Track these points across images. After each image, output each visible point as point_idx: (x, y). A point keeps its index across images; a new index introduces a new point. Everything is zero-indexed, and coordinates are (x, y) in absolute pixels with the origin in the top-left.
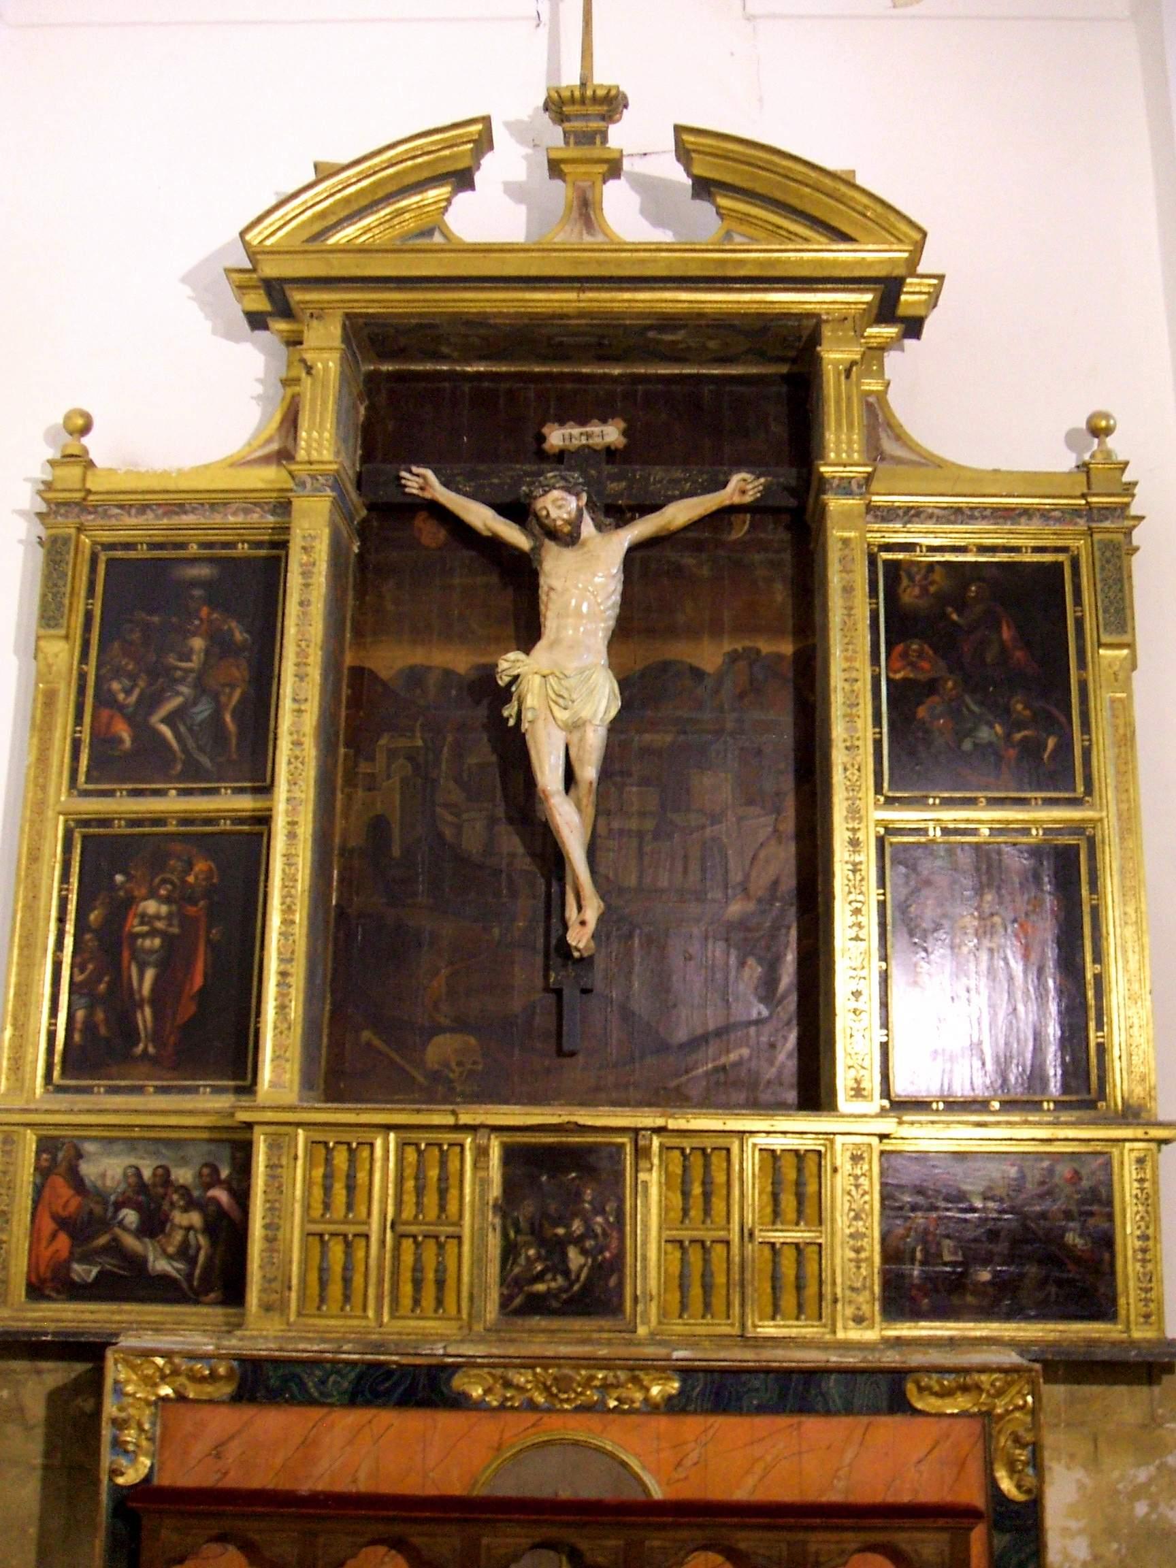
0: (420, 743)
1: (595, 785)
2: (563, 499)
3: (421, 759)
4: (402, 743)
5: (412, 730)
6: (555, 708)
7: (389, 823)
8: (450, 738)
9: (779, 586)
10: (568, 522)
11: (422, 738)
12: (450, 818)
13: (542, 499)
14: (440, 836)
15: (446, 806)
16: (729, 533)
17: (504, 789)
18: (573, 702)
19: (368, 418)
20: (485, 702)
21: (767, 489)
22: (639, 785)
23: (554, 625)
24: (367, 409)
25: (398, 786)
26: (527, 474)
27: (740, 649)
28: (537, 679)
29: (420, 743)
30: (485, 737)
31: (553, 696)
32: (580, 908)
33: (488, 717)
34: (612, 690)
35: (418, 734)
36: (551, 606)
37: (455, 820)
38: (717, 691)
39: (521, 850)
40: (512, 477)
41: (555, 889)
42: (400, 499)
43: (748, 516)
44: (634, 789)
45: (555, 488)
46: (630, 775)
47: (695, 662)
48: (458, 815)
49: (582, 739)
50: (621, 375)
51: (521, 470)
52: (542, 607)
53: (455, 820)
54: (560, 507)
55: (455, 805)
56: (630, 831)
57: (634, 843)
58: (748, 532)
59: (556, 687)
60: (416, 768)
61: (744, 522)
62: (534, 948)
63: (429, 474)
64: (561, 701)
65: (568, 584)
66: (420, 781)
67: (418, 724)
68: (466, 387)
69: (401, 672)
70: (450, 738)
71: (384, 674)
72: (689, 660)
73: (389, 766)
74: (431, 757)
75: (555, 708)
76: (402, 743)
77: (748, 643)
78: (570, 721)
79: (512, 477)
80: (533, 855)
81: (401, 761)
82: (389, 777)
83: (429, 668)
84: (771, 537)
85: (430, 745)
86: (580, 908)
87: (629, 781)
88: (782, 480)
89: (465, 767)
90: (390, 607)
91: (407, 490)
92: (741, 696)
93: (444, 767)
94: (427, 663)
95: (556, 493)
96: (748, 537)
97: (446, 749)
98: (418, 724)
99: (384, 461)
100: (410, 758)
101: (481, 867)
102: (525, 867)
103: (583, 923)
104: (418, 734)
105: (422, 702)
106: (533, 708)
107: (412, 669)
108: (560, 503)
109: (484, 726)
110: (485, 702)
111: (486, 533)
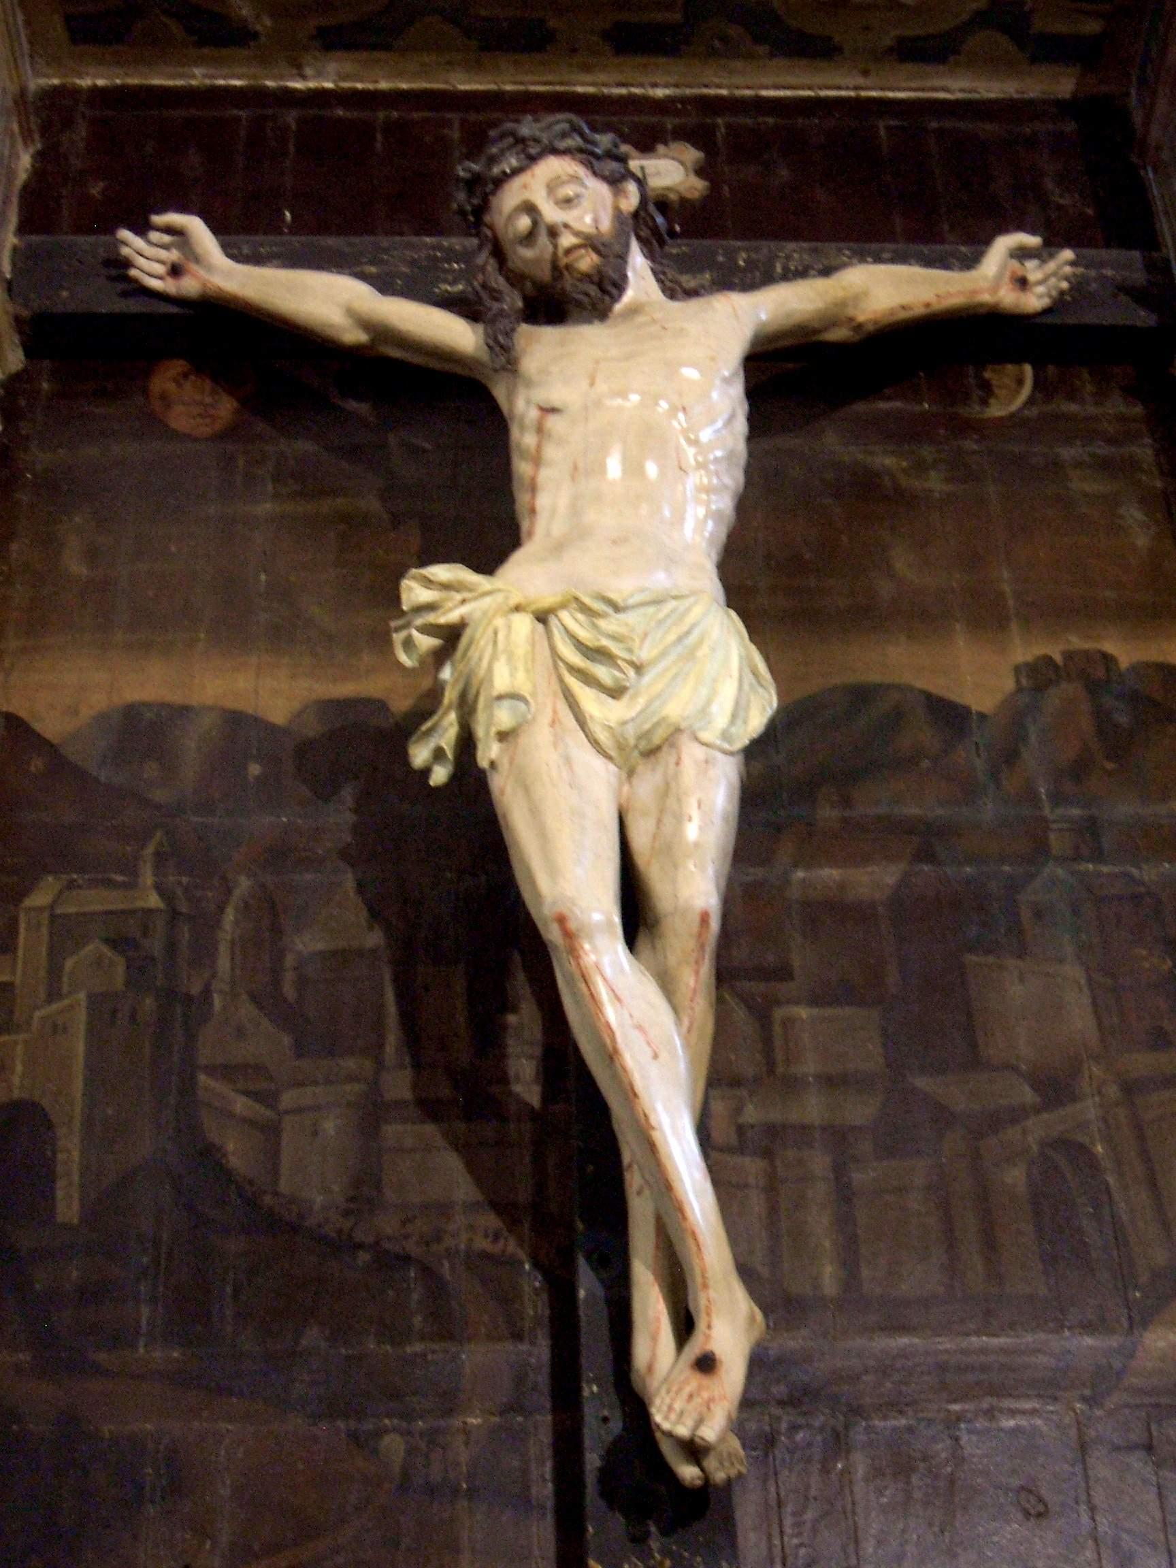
0: (154, 901)
1: (715, 925)
2: (575, 179)
3: (155, 945)
4: (96, 900)
5: (131, 869)
6: (588, 698)
7: (50, 1126)
8: (244, 885)
9: (1133, 514)
10: (591, 242)
11: (159, 888)
12: (241, 1104)
13: (517, 182)
14: (209, 1154)
15: (226, 1071)
16: (984, 402)
17: (408, 1019)
18: (639, 668)
19: (39, 174)
20: (348, 794)
21: (1078, 287)
22: (815, 1000)
23: (563, 502)
24: (39, 156)
25: (82, 1016)
26: (451, 256)
27: (1058, 658)
28: (523, 624)
29: (154, 901)
30: (349, 881)
31: (576, 659)
32: (685, 1325)
33: (355, 829)
34: (747, 661)
35: (148, 877)
36: (551, 452)
37: (262, 1112)
38: (1011, 756)
39: (464, 1189)
40: (413, 263)
41: (587, 1286)
42: (111, 303)
43: (1028, 369)
44: (803, 1012)
45: (555, 151)
46: (783, 973)
47: (939, 686)
48: (267, 1098)
49: (667, 792)
50: (670, 100)
51: (439, 247)
52: (522, 468)
53: (262, 1112)
54: (568, 202)
55: (259, 1069)
56: (804, 1128)
57: (819, 1162)
58: (1031, 401)
59: (584, 634)
60: (139, 970)
61: (1020, 382)
62: (525, 1502)
63: (195, 225)
64: (603, 672)
65: (602, 387)
66: (149, 1002)
67: (150, 849)
68: (291, 118)
69: (102, 718)
70: (244, 885)
71: (51, 726)
72: (920, 684)
73: (55, 971)
74: (185, 934)
75: (588, 698)
76: (96, 900)
77: (1077, 642)
78: (631, 732)
79: (413, 263)
80: (500, 1206)
81: (94, 948)
82: (54, 994)
83: (184, 711)
84: (1091, 410)
85: (184, 908)
86: (685, 1325)
87: (784, 989)
88: (1109, 272)
89: (290, 960)
90: (76, 566)
91: (133, 272)
92: (1079, 769)
93: (224, 963)
94: (175, 697)
95: (552, 167)
96: (1034, 412)
97: (230, 916)
98: (150, 849)
99: (79, 230)
100: (118, 943)
101: (344, 1245)
102: (482, 1244)
103: (706, 1364)
104: (148, 877)
105: (159, 795)
106: (514, 696)
107: (131, 712)
108: (569, 191)
109: (344, 854)
110: (348, 794)
111: (354, 336)
